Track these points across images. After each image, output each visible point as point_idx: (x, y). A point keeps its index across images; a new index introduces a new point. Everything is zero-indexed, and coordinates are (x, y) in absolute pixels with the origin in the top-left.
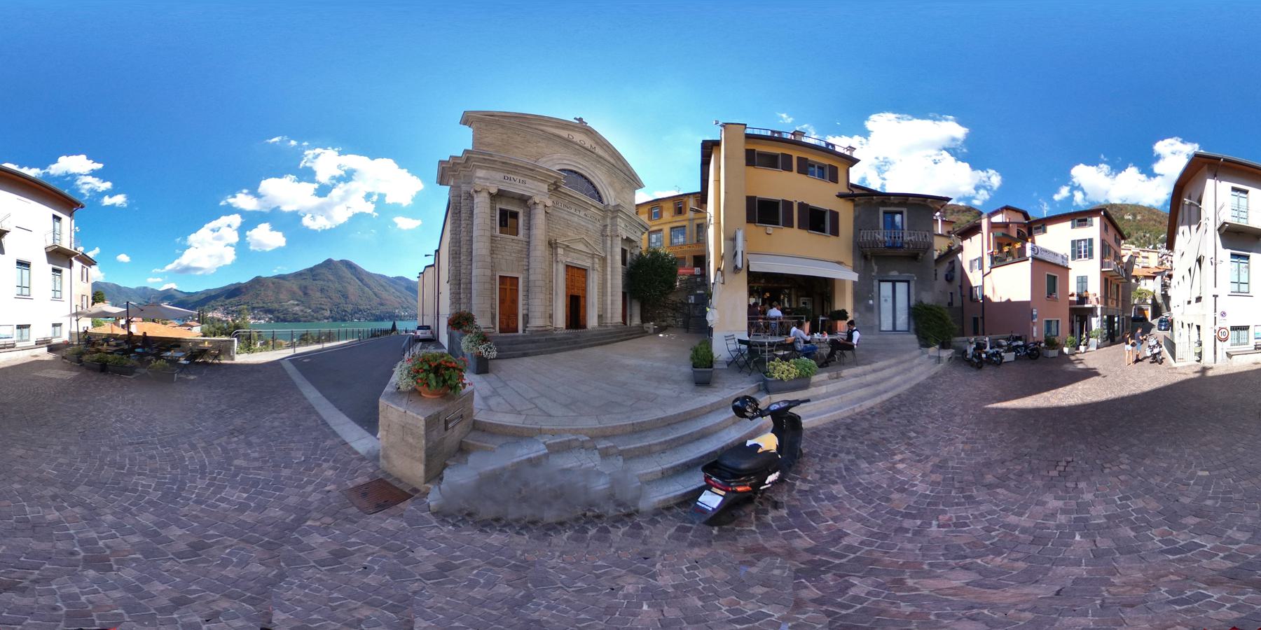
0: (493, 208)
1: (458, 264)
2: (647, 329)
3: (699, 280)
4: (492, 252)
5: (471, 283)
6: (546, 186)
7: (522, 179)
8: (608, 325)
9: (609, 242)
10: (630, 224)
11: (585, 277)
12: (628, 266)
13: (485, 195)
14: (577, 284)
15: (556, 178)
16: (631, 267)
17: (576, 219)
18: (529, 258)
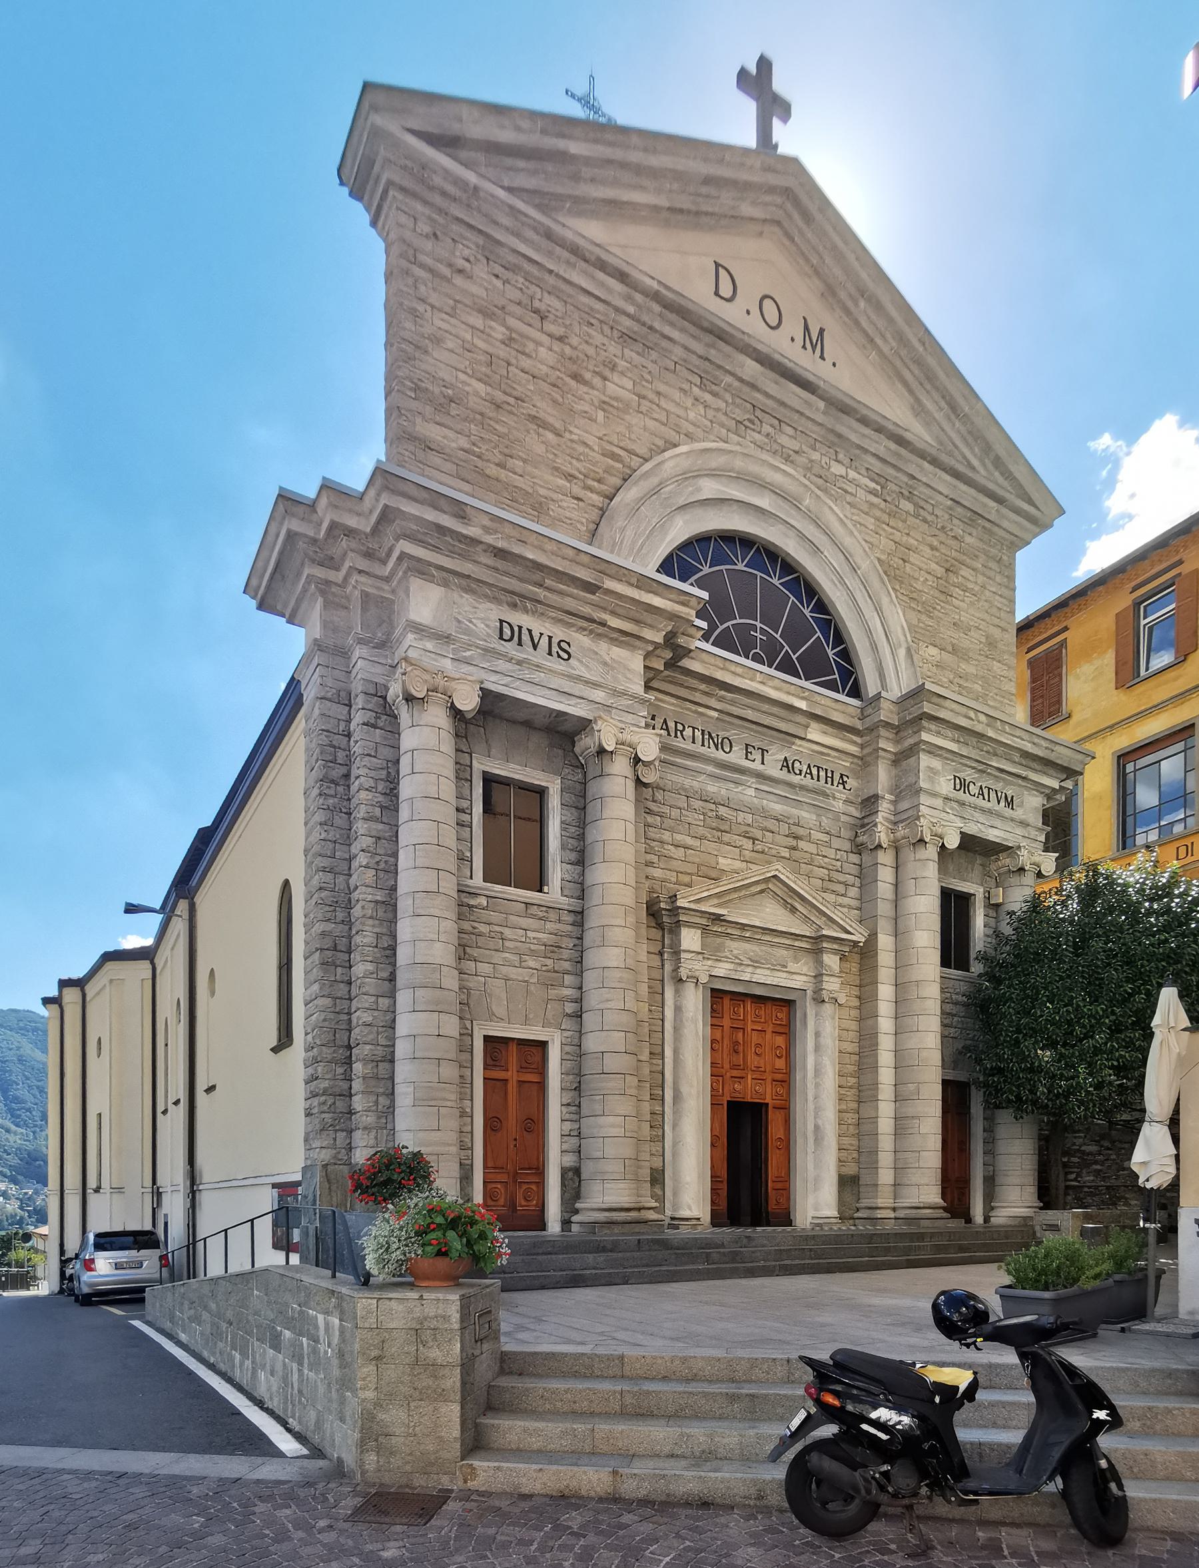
0: (462, 774)
1: (342, 990)
4: (463, 952)
5: (392, 1061)
6: (636, 663)
7: (559, 633)
8: (880, 1214)
10: (983, 769)
11: (787, 1031)
13: (437, 716)
14: (753, 1060)
15: (673, 617)
16: (990, 976)
17: (748, 793)
18: (580, 974)
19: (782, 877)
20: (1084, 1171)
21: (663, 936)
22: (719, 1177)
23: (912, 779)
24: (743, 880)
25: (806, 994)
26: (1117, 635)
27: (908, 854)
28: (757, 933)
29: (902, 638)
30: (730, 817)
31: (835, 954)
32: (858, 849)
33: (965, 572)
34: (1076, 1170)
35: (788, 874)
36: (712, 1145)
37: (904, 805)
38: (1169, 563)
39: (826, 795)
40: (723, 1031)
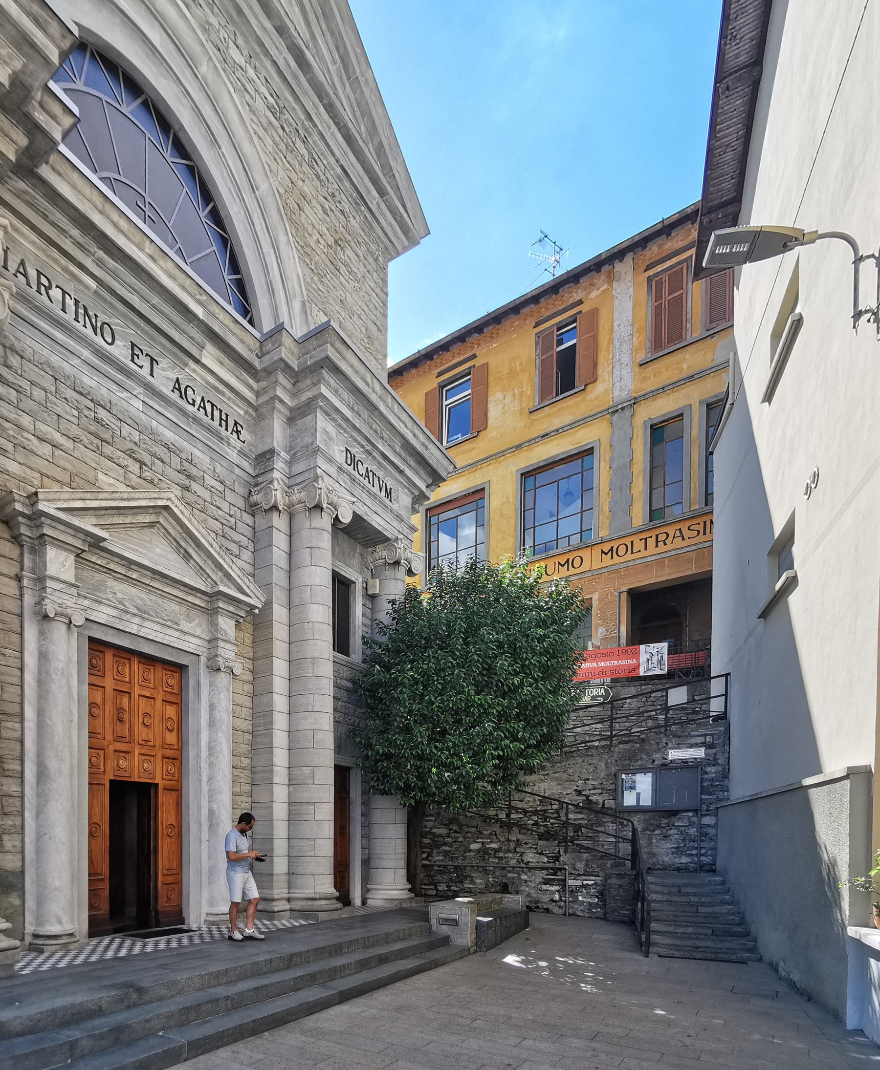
2: (445, 930)
3: (678, 696)
9: (280, 540)
10: (371, 449)
12: (357, 652)
14: (140, 733)
16: (371, 660)
19: (176, 510)
20: (435, 851)
21: (22, 555)
22: (99, 874)
23: (308, 440)
24: (128, 499)
25: (199, 661)
26: (426, 411)
27: (304, 522)
28: (145, 576)
29: (298, 289)
30: (113, 426)
31: (231, 618)
32: (252, 509)
33: (349, 252)
34: (427, 850)
35: (182, 508)
36: (91, 835)
37: (299, 467)
38: (466, 356)
39: (221, 439)
40: (104, 693)
